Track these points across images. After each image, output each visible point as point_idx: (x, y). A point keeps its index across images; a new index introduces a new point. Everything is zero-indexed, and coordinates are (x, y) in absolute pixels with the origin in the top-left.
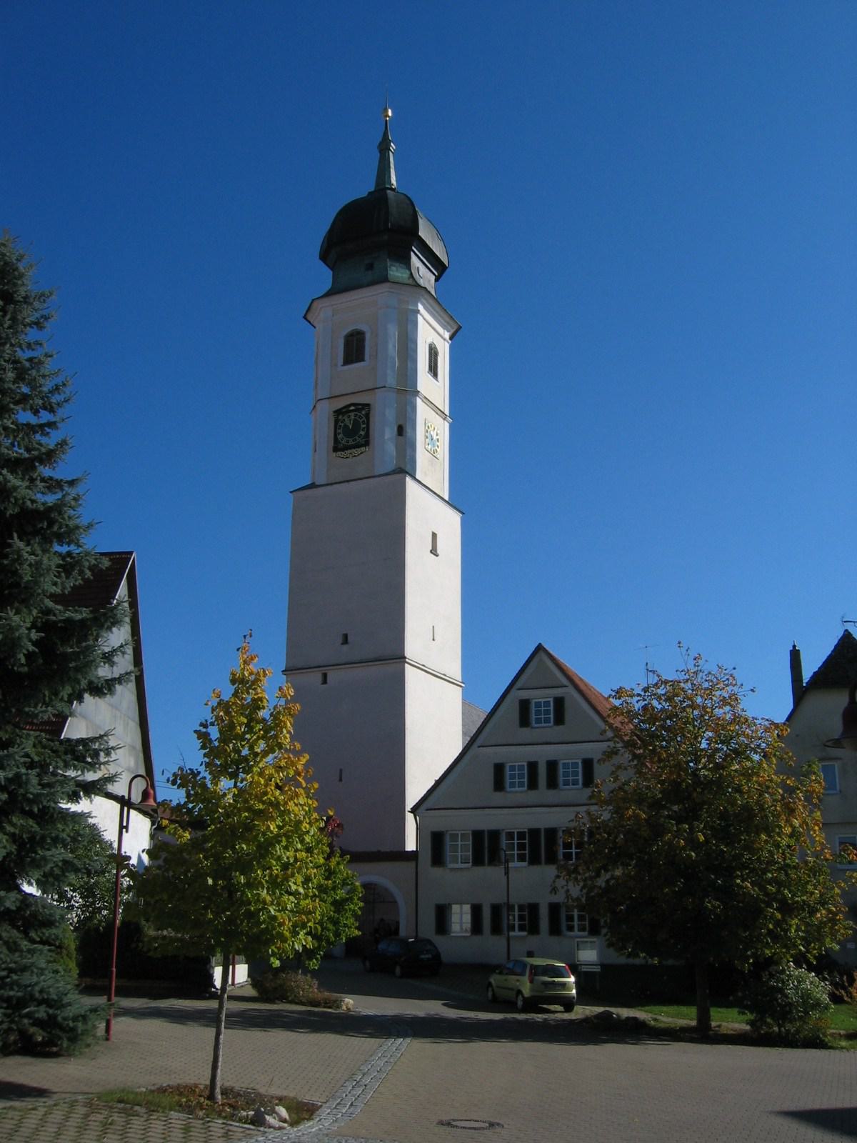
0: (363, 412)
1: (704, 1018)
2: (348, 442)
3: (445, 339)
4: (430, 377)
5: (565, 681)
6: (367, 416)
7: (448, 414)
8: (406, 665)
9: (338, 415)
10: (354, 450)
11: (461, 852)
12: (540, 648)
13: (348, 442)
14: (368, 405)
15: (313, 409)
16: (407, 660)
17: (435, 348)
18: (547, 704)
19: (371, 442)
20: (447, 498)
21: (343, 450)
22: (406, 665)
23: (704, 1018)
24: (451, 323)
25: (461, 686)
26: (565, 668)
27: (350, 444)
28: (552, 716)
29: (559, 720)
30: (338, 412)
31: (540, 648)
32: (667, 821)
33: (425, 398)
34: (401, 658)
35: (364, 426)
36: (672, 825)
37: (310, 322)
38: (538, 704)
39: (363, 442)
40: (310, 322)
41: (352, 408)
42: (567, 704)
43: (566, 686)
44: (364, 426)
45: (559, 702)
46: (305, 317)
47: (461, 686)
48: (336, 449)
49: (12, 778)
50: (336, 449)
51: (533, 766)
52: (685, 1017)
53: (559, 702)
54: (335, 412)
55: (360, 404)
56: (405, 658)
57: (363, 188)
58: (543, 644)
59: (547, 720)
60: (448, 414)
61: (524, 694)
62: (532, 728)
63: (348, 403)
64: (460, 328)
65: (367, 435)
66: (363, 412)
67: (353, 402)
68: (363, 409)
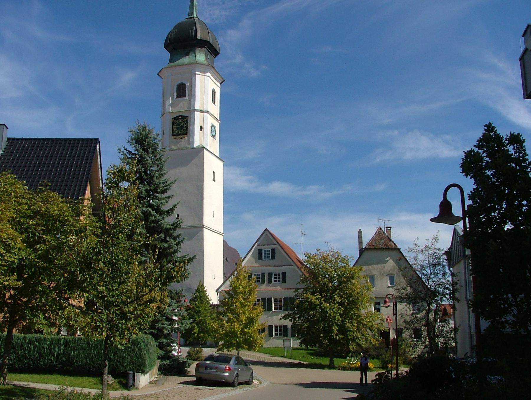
0: (185, 120)
1: (332, 361)
2: (178, 132)
3: (218, 86)
4: (213, 104)
5: (276, 243)
6: (187, 121)
7: (219, 119)
8: (204, 228)
9: (174, 120)
10: (181, 136)
11: (277, 307)
12: (266, 230)
13: (178, 132)
14: (188, 117)
15: (162, 116)
16: (204, 227)
17: (215, 91)
18: (269, 251)
19: (188, 133)
20: (218, 156)
21: (176, 135)
22: (204, 228)
23: (332, 361)
24: (221, 79)
25: (223, 235)
26: (275, 237)
27: (179, 133)
28: (270, 256)
29: (273, 257)
30: (174, 119)
31: (266, 230)
32: (44, 355)
33: (211, 114)
34: (202, 226)
35: (186, 126)
36: (175, 346)
37: (160, 76)
38: (265, 251)
39: (185, 133)
40: (160, 76)
41: (180, 117)
42: (276, 251)
43: (276, 245)
44: (186, 126)
45: (273, 251)
46: (158, 74)
47: (223, 235)
48: (173, 135)
49: (230, 293)
50: (173, 135)
51: (270, 281)
52: (326, 361)
53: (273, 251)
54: (173, 119)
55: (183, 116)
56: (204, 226)
57: (182, 18)
58: (268, 228)
59: (269, 257)
60: (219, 119)
61: (260, 247)
62: (263, 260)
63: (179, 115)
64: (224, 81)
65: (187, 130)
66: (185, 120)
67: (181, 115)
68: (185, 118)
